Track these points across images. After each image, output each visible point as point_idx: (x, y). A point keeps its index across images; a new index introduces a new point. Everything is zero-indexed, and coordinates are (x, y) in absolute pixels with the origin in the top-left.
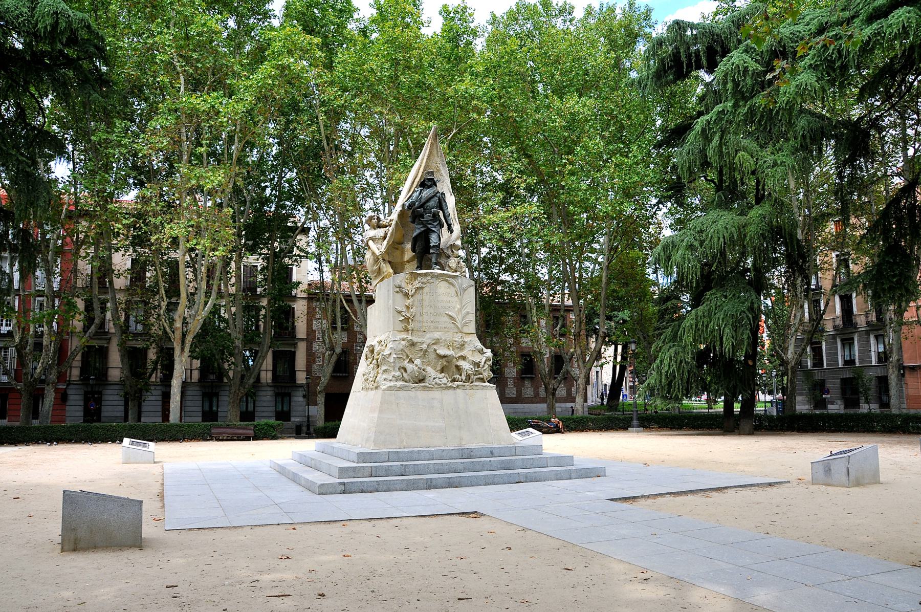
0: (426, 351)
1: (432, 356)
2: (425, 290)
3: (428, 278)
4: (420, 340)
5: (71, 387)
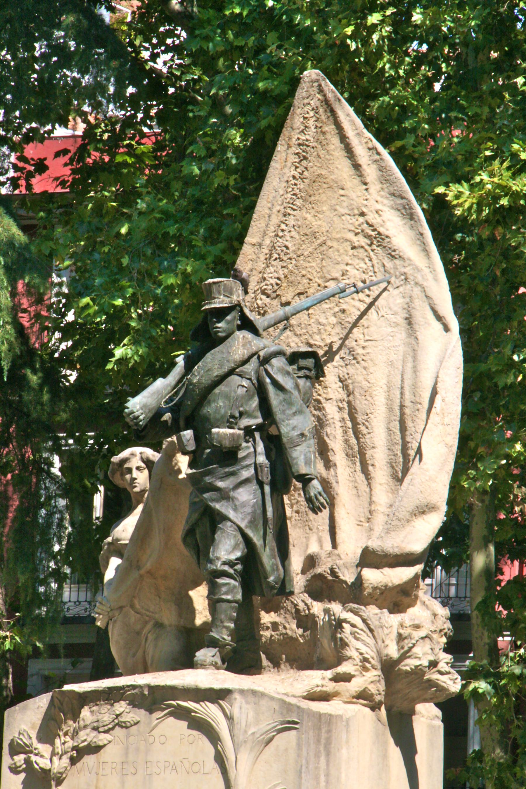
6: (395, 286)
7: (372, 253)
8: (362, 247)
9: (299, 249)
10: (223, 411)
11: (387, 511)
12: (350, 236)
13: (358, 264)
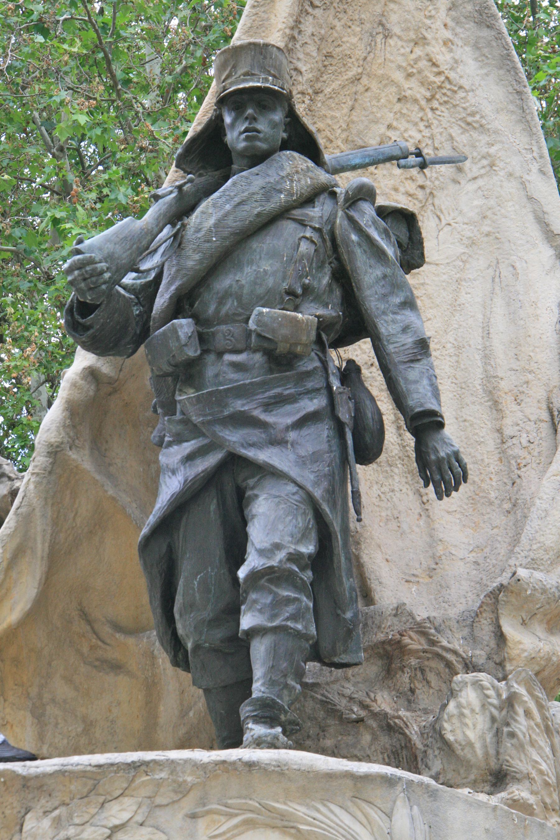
6: (470, 176)
7: (430, 114)
8: (416, 101)
9: (317, 79)
10: (270, 282)
11: (472, 557)
12: (398, 76)
13: (406, 130)
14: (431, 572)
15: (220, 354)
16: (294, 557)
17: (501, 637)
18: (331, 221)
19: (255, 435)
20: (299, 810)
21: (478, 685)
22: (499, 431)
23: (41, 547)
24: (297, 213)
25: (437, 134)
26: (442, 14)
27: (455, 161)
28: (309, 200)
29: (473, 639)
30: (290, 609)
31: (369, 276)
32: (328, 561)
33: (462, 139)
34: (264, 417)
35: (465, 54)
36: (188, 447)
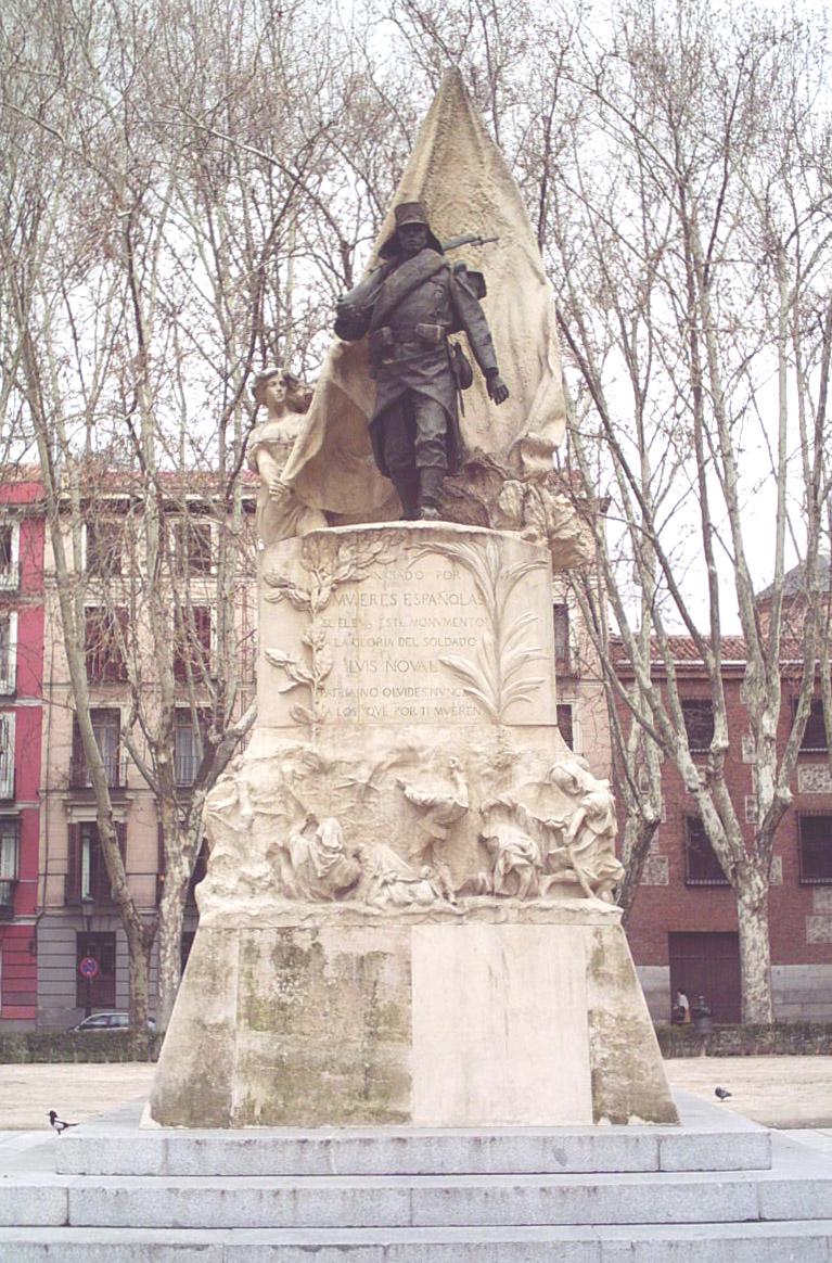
0: (368, 788)
1: (386, 805)
2: (364, 587)
3: (377, 547)
4: (348, 755)
5: (44, 922)
12: (469, 202)
14: (488, 429)
15: (402, 343)
16: (439, 436)
17: (522, 463)
18: (449, 280)
19: (419, 380)
20: (446, 545)
21: (513, 485)
22: (517, 364)
23: (322, 424)
24: (433, 278)
25: (488, 228)
26: (487, 174)
27: (495, 240)
28: (438, 272)
29: (508, 462)
30: (438, 458)
31: (464, 304)
32: (452, 437)
33: (497, 229)
34: (424, 372)
35: (497, 191)
36: (389, 384)
